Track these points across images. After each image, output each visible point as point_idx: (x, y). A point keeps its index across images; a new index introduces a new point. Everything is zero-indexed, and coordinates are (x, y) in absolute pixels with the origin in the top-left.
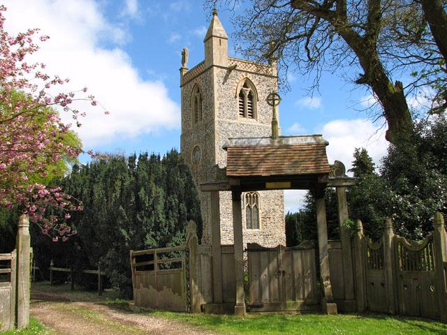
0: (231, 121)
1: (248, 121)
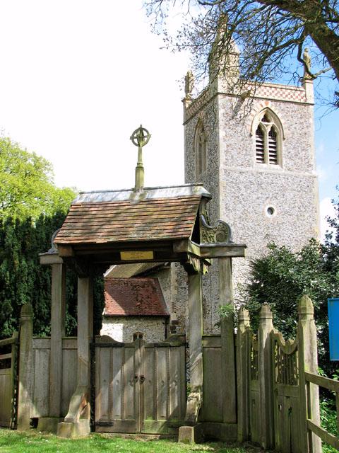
0: (243, 169)
1: (268, 167)
